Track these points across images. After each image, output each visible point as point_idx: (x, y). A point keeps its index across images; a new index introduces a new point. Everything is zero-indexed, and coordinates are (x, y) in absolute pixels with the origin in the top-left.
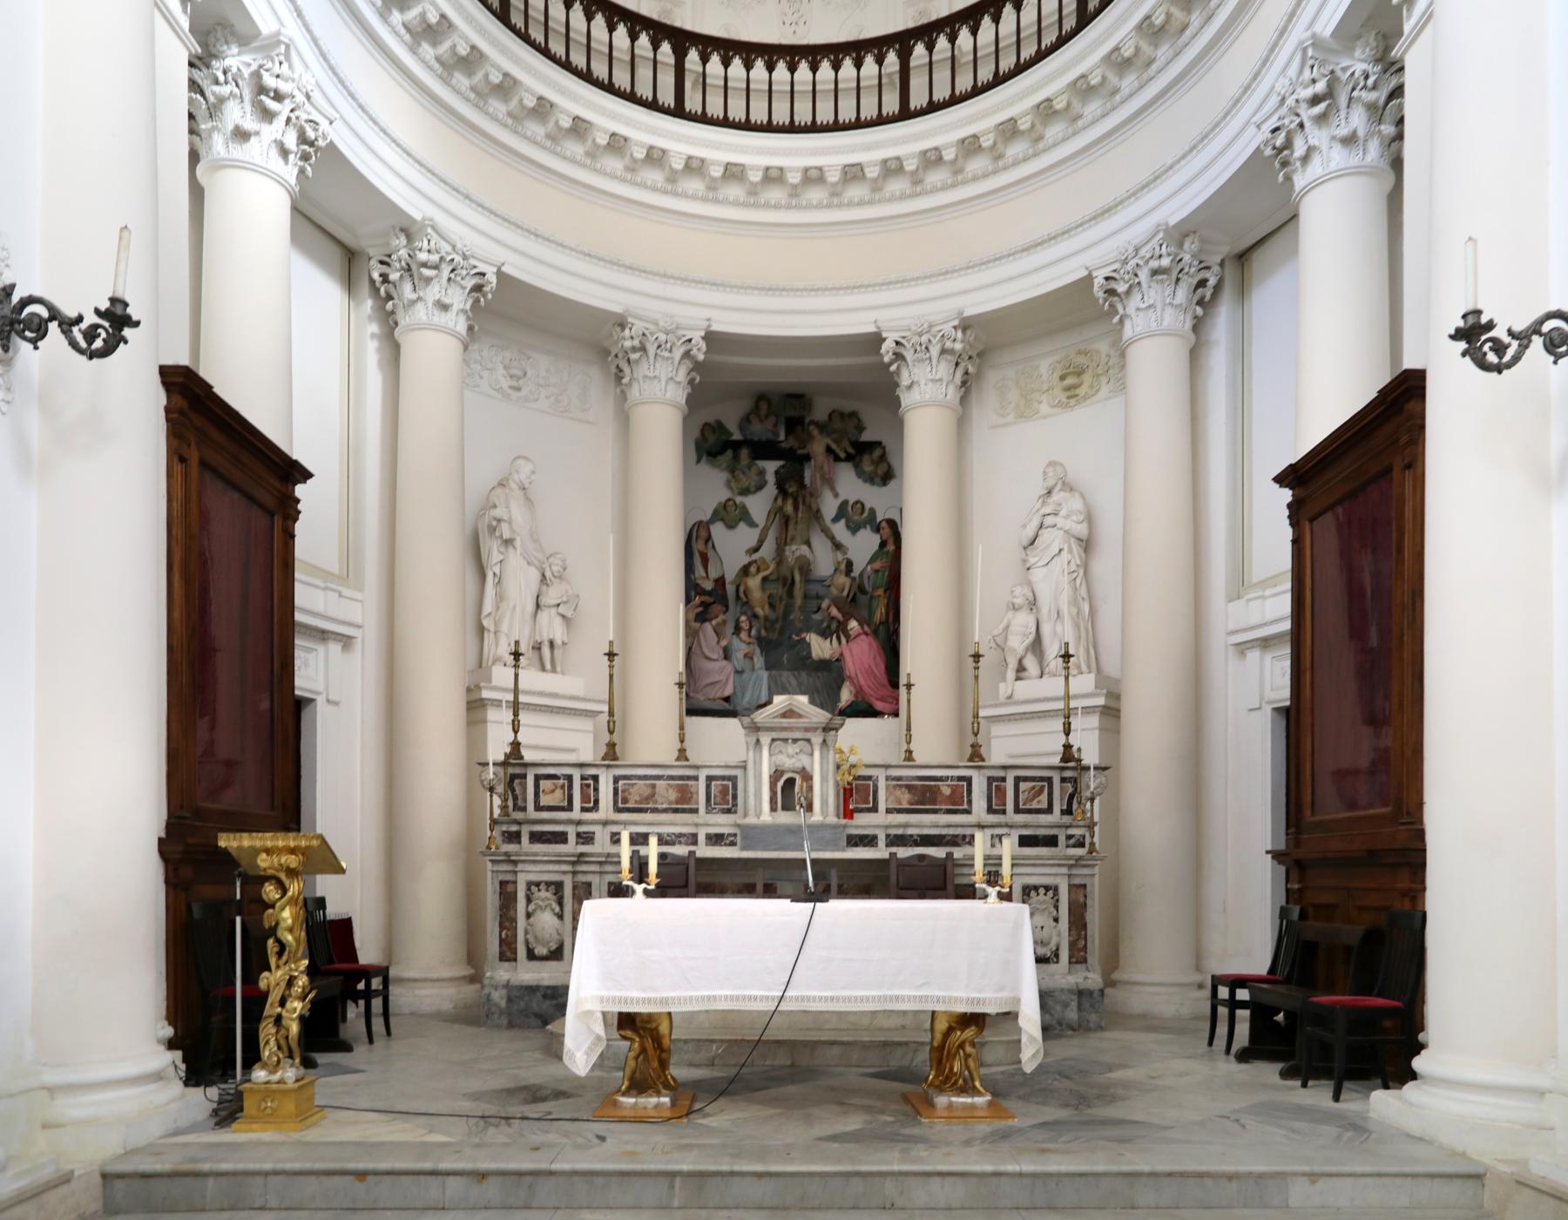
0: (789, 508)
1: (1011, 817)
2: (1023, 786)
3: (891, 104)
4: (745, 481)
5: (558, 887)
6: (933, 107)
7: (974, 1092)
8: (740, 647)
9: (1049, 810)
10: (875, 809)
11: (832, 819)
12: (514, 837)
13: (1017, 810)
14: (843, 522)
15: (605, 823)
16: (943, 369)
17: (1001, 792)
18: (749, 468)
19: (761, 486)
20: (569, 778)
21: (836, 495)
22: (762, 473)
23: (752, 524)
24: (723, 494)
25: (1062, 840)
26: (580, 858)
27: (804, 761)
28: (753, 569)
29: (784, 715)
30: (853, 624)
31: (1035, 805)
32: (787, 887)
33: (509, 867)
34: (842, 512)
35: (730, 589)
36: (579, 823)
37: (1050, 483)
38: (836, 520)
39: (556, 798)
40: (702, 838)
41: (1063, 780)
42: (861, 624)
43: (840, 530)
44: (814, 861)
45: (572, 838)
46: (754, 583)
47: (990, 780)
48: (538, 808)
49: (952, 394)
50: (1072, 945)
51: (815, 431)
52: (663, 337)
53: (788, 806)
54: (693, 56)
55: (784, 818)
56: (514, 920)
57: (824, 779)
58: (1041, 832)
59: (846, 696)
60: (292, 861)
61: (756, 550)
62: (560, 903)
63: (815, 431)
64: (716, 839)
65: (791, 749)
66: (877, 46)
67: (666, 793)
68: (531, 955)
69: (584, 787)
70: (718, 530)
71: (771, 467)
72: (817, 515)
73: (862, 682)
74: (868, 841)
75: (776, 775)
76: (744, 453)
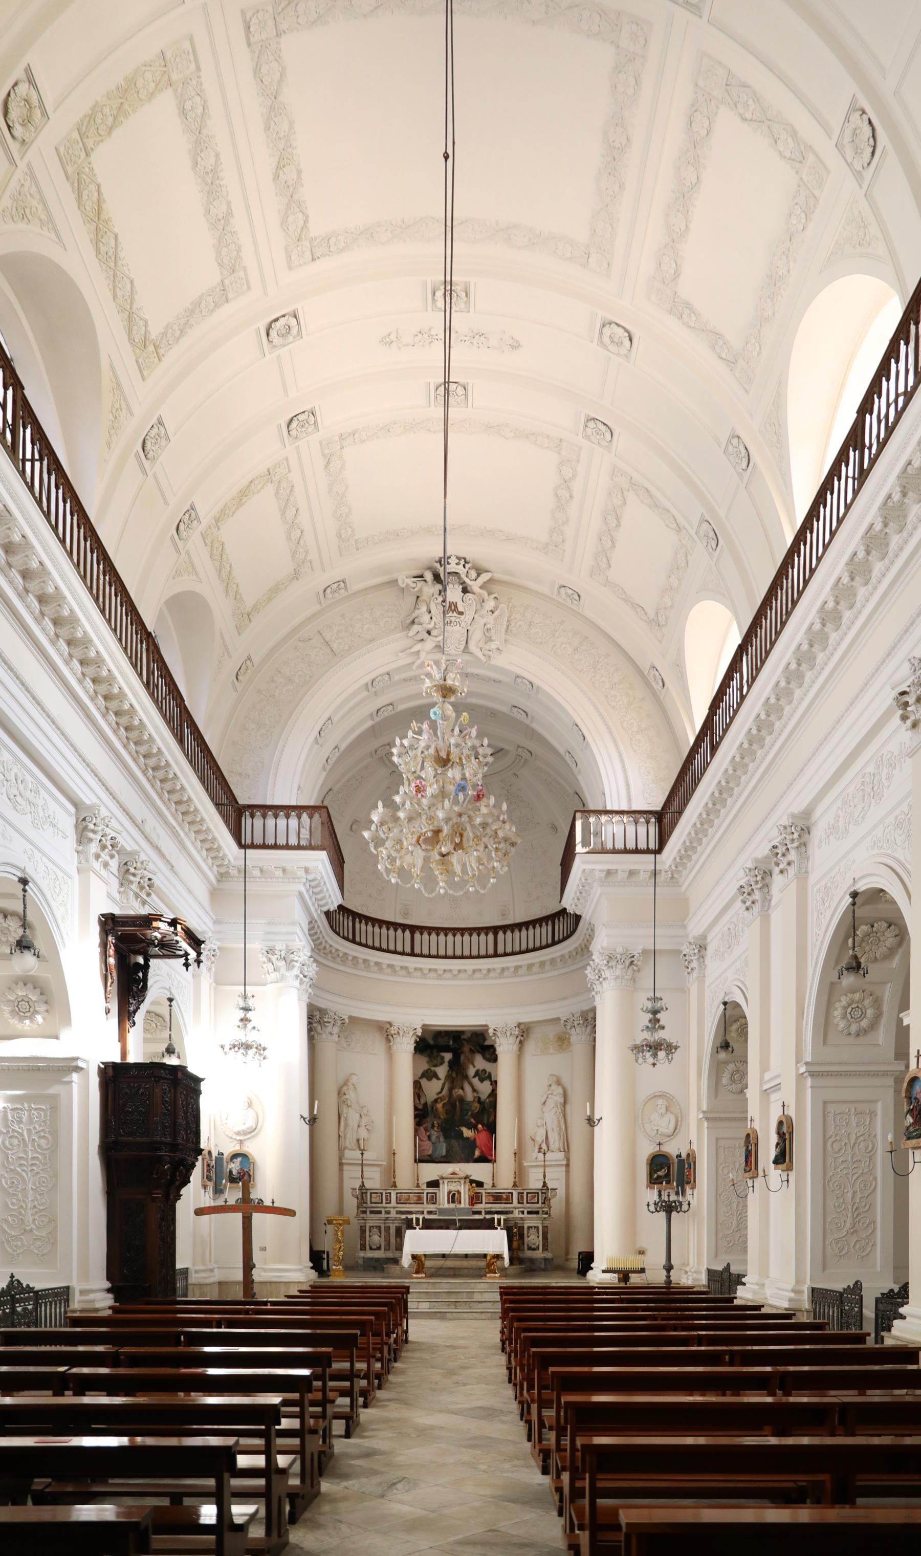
0: (454, 1075)
1: (525, 1205)
2: (529, 1195)
3: (491, 951)
4: (435, 1062)
5: (379, 1228)
6: (505, 954)
7: (495, 1273)
8: (435, 1134)
9: (538, 1203)
10: (481, 1203)
11: (468, 1206)
12: (365, 1212)
13: (527, 1203)
14: (477, 1078)
15: (394, 1208)
16: (512, 1040)
17: (522, 1197)
18: (437, 1057)
19: (442, 1063)
20: (382, 1193)
21: (474, 1067)
22: (443, 1058)
23: (438, 1079)
24: (425, 1066)
25: (541, 1212)
26: (387, 1219)
27: (459, 1188)
28: (439, 1101)
29: (452, 1174)
30: (480, 1126)
31: (533, 1201)
32: (452, 1226)
33: (363, 1221)
34: (477, 1074)
35: (429, 1108)
36: (386, 1208)
37: (550, 1083)
38: (474, 1077)
39: (378, 1200)
40: (425, 1212)
41: (542, 1193)
42: (483, 1126)
43: (476, 1081)
44: (459, 1220)
45: (383, 1212)
46: (439, 1106)
47: (519, 1193)
48: (371, 1203)
49: (515, 1047)
50: (543, 1245)
51: (465, 1043)
52: (406, 1029)
53: (453, 1202)
54: (417, 936)
55: (452, 1206)
56: (365, 1238)
57: (465, 1193)
58: (534, 1210)
59: (477, 1153)
60: (341, 1222)
61: (441, 1092)
62: (380, 1232)
63: (465, 1043)
64: (430, 1213)
65: (454, 1184)
66: (486, 930)
67: (413, 1198)
68: (371, 1249)
69: (386, 1196)
70: (424, 1082)
71: (448, 1056)
72: (466, 1077)
73: (483, 1149)
74: (479, 1213)
75: (449, 1192)
76: (435, 1051)
